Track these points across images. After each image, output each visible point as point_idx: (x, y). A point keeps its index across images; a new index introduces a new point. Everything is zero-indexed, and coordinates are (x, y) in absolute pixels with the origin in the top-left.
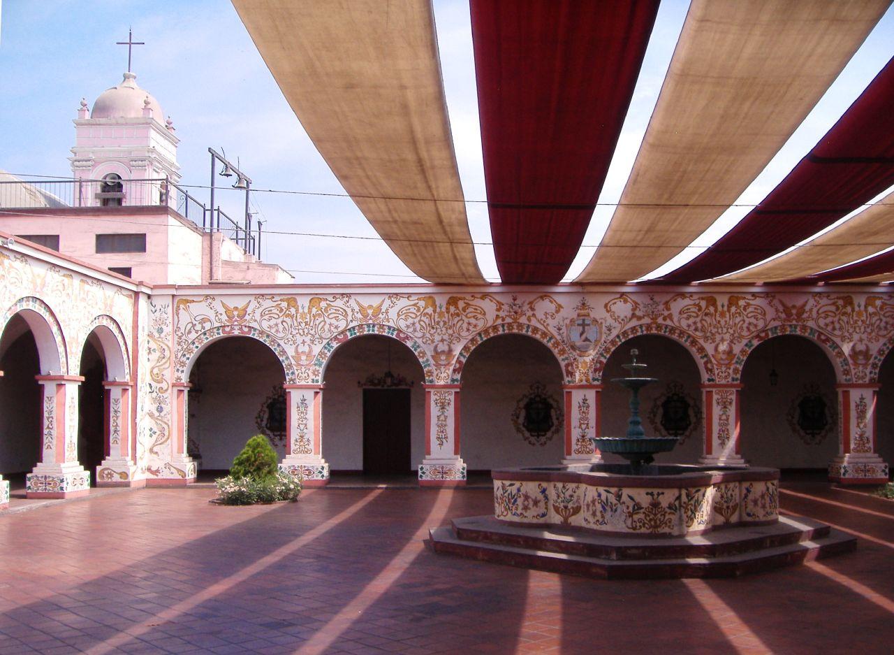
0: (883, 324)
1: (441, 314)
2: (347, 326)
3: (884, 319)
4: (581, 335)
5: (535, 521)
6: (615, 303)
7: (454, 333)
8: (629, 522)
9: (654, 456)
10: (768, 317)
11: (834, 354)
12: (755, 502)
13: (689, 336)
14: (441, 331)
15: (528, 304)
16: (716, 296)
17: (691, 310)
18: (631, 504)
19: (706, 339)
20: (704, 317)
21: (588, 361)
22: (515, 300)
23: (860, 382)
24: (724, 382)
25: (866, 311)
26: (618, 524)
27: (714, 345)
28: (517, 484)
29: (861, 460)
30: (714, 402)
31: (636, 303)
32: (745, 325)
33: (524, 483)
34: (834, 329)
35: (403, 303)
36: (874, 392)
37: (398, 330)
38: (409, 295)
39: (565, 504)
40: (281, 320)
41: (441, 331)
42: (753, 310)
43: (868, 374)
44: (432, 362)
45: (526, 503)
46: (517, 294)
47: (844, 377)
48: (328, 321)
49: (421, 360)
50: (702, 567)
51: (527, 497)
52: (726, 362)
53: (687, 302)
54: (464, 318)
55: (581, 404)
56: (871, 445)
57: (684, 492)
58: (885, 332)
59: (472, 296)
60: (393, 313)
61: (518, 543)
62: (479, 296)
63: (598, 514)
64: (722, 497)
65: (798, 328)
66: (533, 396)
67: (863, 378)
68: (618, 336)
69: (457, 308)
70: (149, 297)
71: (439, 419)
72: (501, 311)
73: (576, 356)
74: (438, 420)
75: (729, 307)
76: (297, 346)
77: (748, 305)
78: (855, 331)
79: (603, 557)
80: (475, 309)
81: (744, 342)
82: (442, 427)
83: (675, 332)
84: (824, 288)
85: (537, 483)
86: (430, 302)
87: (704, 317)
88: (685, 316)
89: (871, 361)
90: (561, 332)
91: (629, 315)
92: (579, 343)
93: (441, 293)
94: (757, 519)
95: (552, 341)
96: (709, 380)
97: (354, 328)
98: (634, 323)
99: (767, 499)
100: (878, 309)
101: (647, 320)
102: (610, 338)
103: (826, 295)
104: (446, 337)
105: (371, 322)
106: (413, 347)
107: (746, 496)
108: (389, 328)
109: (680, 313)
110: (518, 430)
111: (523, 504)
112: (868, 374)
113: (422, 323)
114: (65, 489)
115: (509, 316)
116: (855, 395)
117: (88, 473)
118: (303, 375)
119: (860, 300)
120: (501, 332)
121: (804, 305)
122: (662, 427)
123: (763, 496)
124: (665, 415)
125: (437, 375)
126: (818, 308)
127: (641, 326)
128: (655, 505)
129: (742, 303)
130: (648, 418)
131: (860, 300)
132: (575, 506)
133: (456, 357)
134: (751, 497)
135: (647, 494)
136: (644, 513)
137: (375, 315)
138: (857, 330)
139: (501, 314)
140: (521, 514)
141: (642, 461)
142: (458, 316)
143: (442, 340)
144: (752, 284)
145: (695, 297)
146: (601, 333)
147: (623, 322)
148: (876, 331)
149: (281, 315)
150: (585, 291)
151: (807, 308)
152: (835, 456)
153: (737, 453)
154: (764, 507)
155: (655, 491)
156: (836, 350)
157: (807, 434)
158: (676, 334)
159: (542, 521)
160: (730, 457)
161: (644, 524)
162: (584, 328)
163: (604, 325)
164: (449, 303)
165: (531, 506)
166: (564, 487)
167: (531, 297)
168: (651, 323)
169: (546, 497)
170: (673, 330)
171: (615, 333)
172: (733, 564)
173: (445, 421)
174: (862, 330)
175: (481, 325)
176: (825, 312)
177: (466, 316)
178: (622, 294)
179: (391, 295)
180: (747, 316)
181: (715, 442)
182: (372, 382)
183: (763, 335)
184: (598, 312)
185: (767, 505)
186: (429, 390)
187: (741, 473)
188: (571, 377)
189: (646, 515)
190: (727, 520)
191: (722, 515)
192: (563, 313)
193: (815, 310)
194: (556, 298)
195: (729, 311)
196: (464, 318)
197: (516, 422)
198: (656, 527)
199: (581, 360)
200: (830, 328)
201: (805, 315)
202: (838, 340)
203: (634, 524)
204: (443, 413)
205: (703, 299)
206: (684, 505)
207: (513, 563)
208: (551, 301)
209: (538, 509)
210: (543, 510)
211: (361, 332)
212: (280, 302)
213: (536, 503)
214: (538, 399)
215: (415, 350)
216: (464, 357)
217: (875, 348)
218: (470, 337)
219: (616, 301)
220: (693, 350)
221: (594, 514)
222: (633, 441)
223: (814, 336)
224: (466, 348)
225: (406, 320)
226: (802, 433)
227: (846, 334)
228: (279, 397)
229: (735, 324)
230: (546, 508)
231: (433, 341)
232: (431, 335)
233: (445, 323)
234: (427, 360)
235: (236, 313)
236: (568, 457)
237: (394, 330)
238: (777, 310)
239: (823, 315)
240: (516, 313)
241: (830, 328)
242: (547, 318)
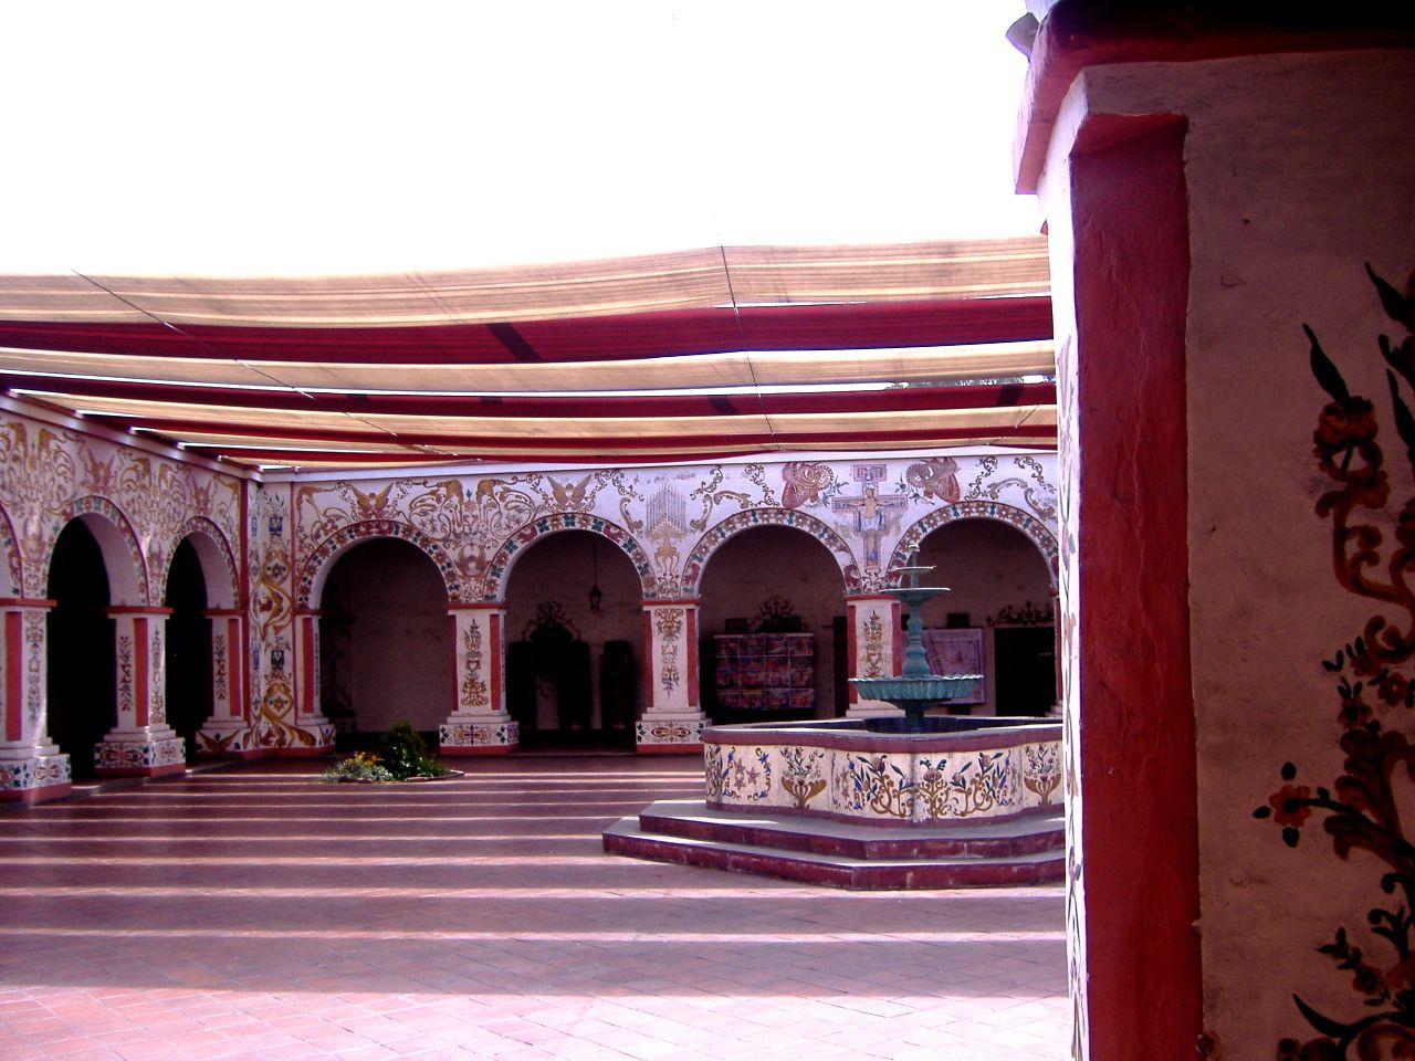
5: (751, 802)
17: (427, 502)
42: (514, 498)
45: (739, 776)
48: (505, 512)
60: (403, 505)
63: (851, 793)
66: (767, 617)
69: (492, 496)
70: (260, 485)
75: (479, 495)
76: (462, 549)
80: (517, 497)
114: (150, 762)
117: (181, 740)
166: (1041, 749)
195: (479, 502)
214: (551, 625)
221: (845, 794)
230: (768, 784)
236: (453, 713)
241: (429, 527)
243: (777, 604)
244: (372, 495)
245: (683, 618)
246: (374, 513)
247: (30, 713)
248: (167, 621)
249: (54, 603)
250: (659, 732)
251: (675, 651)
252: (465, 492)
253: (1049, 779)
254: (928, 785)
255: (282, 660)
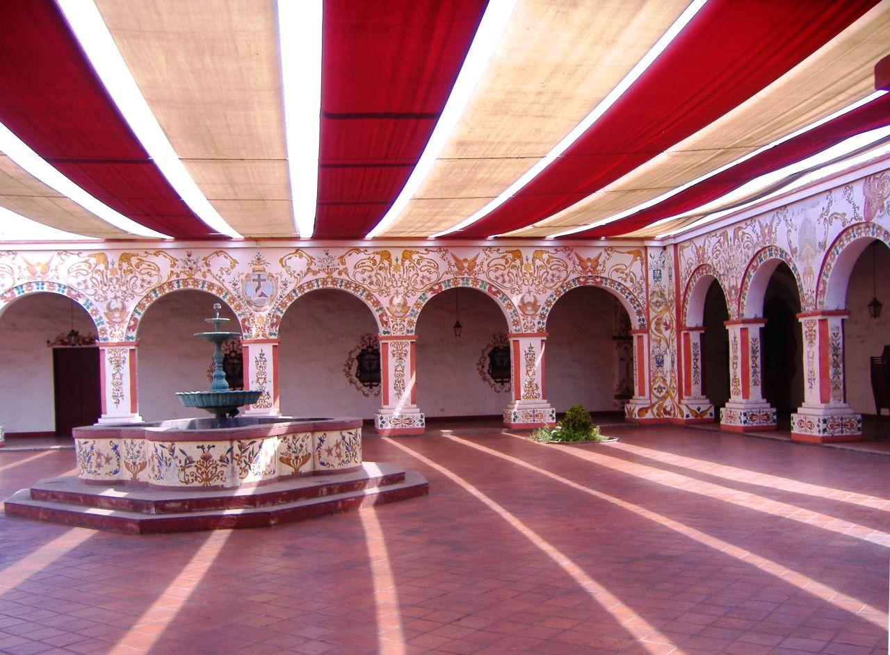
0: (550, 277)
1: (113, 271)
2: (14, 284)
3: (551, 272)
4: (257, 290)
5: (108, 478)
6: (291, 258)
7: (128, 290)
8: (182, 475)
9: (239, 409)
10: (441, 271)
11: (504, 305)
12: (329, 451)
13: (365, 290)
14: (114, 288)
15: (203, 260)
16: (390, 251)
18: (183, 458)
19: (381, 292)
20: (379, 271)
21: (265, 316)
22: (189, 256)
23: (529, 332)
24: (399, 334)
25: (534, 264)
26: (172, 478)
27: (388, 298)
28: (91, 441)
29: (531, 406)
30: (390, 355)
31: (311, 258)
32: (419, 279)
33: (96, 440)
34: (504, 281)
35: (74, 259)
36: (543, 341)
37: (69, 287)
38: (80, 252)
39: (134, 460)
40: (90, 276)
41: (114, 288)
42: (426, 263)
43: (536, 324)
44: (105, 319)
45: (99, 460)
46: (191, 250)
47: (514, 327)
49: (94, 318)
50: (235, 517)
51: (99, 455)
52: (402, 314)
53: (362, 256)
54: (138, 274)
55: (258, 359)
56: (540, 391)
57: (236, 444)
58: (552, 285)
59: (146, 253)
60: (63, 271)
61: (79, 500)
62: (153, 252)
63: (156, 469)
64: (289, 447)
65: (470, 282)
67: (531, 328)
68: (294, 291)
71: (114, 377)
72: (176, 267)
73: (252, 311)
74: (114, 378)
75: (403, 261)
77: (422, 258)
78: (523, 283)
79: (145, 511)
80: (428, 262)
81: (419, 294)
82: (118, 385)
83: (350, 286)
84: (310, 242)
85: (109, 440)
86: (102, 258)
87: (379, 271)
88: (360, 270)
89: (540, 311)
90: (237, 287)
91: (305, 270)
92: (255, 298)
93: (177, 249)
94: (331, 468)
95: (228, 297)
96: (385, 333)
97: (21, 286)
98: (310, 277)
99: (343, 449)
100: (545, 262)
101: (322, 275)
102: (286, 293)
103: (77, 253)
104: (119, 294)
105: (39, 279)
106: (85, 304)
107: (319, 446)
108: (60, 285)
109: (355, 267)
110: (484, 379)
111: (97, 462)
112: (536, 324)
113: (94, 280)
115: (184, 272)
116: (524, 344)
118: (399, 327)
119: (528, 253)
120: (176, 288)
121: (475, 259)
122: (357, 380)
123: (337, 445)
124: (360, 368)
125: (111, 332)
126: (488, 261)
127: (317, 281)
128: (206, 458)
129: (415, 257)
130: (344, 371)
131: (528, 253)
132: (142, 462)
133: (131, 314)
134: (324, 446)
135: (198, 447)
136: (196, 466)
137: (44, 273)
138: (526, 282)
139: (176, 270)
140: (95, 471)
141: (227, 415)
142: (132, 273)
143: (116, 298)
144: (424, 239)
145: (370, 251)
146: (277, 288)
147: (298, 277)
148: (543, 283)
149: (90, 271)
150: (259, 246)
151: (478, 262)
152: (508, 403)
153: (413, 402)
154: (339, 456)
155: (206, 444)
156: (506, 302)
157: (364, 386)
158: (352, 288)
159: (114, 477)
160: (406, 407)
161: (196, 477)
162: (259, 284)
163: (279, 280)
164: (121, 260)
165: (103, 463)
166: (132, 443)
167: (206, 253)
168: (327, 277)
169: (118, 454)
170: (348, 284)
171: (290, 287)
172: (269, 513)
173: (121, 379)
174: (531, 282)
175: (155, 282)
176: (495, 265)
177: (140, 273)
178: (298, 249)
179: (60, 252)
180: (420, 270)
181: (392, 392)
182: (63, 343)
183: (436, 287)
184: (274, 268)
185: (343, 454)
186: (104, 348)
187: (314, 424)
188: (248, 332)
189: (198, 468)
190: (297, 470)
191: (290, 465)
192: (238, 268)
193: (486, 263)
194: (231, 253)
195: (403, 264)
196: (138, 274)
197: (482, 373)
198: (208, 480)
199: (257, 315)
200: (500, 281)
201: (476, 269)
202: (507, 292)
203: (186, 477)
204: (118, 372)
205: (377, 253)
206: (237, 457)
207: (67, 521)
208: (225, 257)
209: (109, 466)
210: (115, 467)
211: (29, 290)
212: (505, 254)
213: (108, 460)
214: (233, 355)
215: (88, 307)
216: (139, 314)
217: (542, 299)
218: (145, 294)
219: (291, 256)
220: (369, 304)
222: (218, 394)
223: (485, 288)
224: (139, 305)
225: (77, 277)
226: (492, 381)
227: (516, 286)
228: (231, 352)
229: (409, 277)
230: (119, 465)
231: (106, 299)
232: (104, 292)
233: (118, 280)
234: (101, 318)
235: (589, 264)
237: (65, 287)
238: (450, 264)
239: (494, 268)
240: (190, 268)
241: (500, 281)
242: (222, 274)
243: (370, 339)
244: (39, 264)
245: (127, 355)
246: (466, 272)
247: (810, 385)
248: (761, 329)
249: (766, 320)
250: (801, 424)
251: (121, 377)
252: (524, 257)
253: (137, 463)
254: (203, 462)
255: (662, 362)
